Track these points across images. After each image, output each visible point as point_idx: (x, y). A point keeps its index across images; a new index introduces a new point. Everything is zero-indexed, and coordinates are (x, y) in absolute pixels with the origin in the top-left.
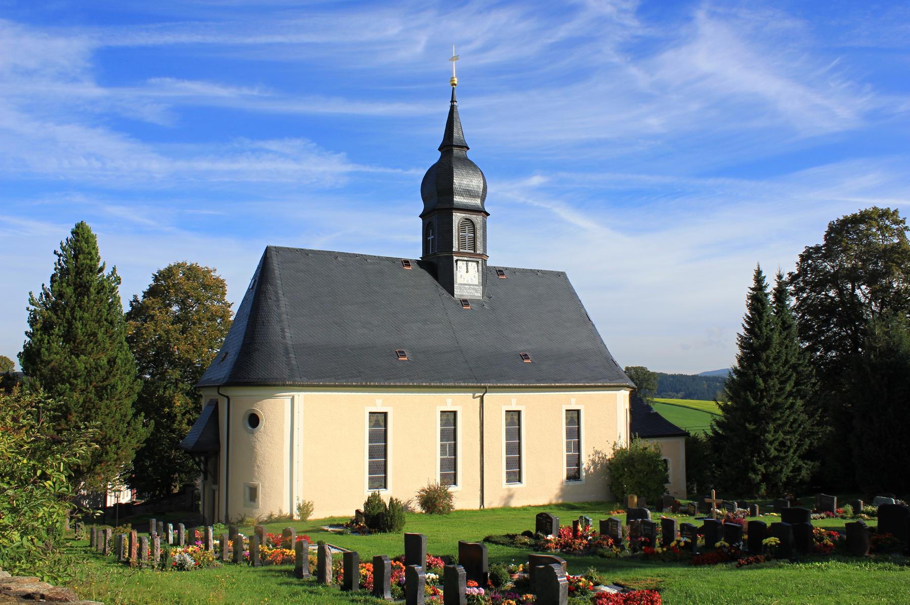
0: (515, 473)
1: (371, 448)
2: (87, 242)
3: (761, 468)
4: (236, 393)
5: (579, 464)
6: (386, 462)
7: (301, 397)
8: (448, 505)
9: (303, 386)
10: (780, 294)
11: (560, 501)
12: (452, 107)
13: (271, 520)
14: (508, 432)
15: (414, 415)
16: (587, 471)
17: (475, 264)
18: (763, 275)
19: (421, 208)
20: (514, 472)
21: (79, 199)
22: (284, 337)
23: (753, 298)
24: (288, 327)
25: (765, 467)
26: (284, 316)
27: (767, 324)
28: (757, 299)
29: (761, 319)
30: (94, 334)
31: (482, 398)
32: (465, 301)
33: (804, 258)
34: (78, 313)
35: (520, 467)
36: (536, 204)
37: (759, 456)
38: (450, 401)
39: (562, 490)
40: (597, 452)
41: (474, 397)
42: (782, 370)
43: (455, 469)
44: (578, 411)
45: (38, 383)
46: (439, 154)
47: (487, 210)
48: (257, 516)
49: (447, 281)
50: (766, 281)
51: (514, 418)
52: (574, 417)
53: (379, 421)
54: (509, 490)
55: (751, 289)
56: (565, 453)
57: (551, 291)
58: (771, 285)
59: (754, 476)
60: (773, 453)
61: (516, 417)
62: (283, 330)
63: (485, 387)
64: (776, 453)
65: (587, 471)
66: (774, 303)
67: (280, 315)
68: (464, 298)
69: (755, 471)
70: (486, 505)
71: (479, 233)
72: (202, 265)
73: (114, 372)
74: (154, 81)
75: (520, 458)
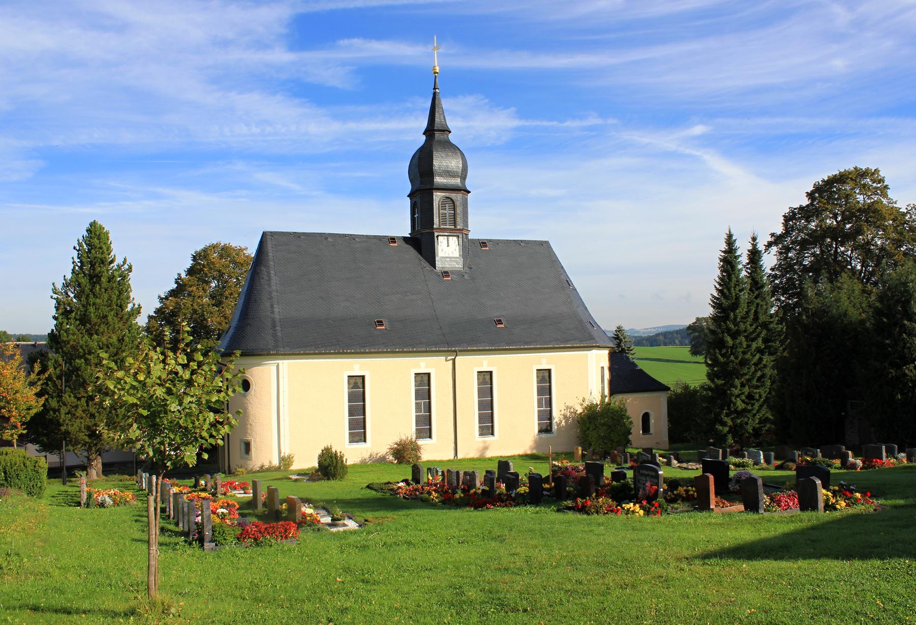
0: (487, 425)
1: (350, 407)
2: (99, 239)
5: (550, 418)
6: (364, 419)
7: (286, 364)
9: (285, 355)
10: (755, 255)
11: (534, 452)
12: (435, 94)
13: (262, 470)
15: (390, 378)
16: (558, 425)
17: (455, 238)
18: (734, 238)
19: (408, 188)
21: (240, 166)
22: (273, 312)
23: (725, 261)
24: (280, 303)
25: (732, 419)
26: (274, 293)
27: (736, 285)
28: (729, 261)
29: (731, 281)
30: (105, 317)
31: (454, 360)
32: (445, 272)
33: (787, 219)
34: (92, 300)
35: (492, 422)
36: (688, 151)
37: (729, 409)
38: (423, 364)
39: (536, 442)
40: (567, 407)
41: (446, 360)
42: (750, 329)
43: (430, 424)
44: (549, 371)
45: (60, 359)
46: (424, 138)
47: (469, 189)
48: (251, 467)
49: (429, 254)
50: (737, 244)
51: (486, 379)
52: (545, 377)
53: (357, 385)
54: (484, 442)
56: (536, 409)
57: (535, 260)
58: (743, 250)
59: (721, 428)
60: (740, 405)
61: (488, 377)
62: (272, 306)
63: (455, 351)
64: (744, 406)
65: (558, 425)
66: (748, 264)
67: (270, 293)
68: (446, 270)
69: (724, 424)
70: (460, 456)
71: (459, 210)
72: (234, 244)
73: (123, 348)
74: (345, 42)
75: (492, 413)
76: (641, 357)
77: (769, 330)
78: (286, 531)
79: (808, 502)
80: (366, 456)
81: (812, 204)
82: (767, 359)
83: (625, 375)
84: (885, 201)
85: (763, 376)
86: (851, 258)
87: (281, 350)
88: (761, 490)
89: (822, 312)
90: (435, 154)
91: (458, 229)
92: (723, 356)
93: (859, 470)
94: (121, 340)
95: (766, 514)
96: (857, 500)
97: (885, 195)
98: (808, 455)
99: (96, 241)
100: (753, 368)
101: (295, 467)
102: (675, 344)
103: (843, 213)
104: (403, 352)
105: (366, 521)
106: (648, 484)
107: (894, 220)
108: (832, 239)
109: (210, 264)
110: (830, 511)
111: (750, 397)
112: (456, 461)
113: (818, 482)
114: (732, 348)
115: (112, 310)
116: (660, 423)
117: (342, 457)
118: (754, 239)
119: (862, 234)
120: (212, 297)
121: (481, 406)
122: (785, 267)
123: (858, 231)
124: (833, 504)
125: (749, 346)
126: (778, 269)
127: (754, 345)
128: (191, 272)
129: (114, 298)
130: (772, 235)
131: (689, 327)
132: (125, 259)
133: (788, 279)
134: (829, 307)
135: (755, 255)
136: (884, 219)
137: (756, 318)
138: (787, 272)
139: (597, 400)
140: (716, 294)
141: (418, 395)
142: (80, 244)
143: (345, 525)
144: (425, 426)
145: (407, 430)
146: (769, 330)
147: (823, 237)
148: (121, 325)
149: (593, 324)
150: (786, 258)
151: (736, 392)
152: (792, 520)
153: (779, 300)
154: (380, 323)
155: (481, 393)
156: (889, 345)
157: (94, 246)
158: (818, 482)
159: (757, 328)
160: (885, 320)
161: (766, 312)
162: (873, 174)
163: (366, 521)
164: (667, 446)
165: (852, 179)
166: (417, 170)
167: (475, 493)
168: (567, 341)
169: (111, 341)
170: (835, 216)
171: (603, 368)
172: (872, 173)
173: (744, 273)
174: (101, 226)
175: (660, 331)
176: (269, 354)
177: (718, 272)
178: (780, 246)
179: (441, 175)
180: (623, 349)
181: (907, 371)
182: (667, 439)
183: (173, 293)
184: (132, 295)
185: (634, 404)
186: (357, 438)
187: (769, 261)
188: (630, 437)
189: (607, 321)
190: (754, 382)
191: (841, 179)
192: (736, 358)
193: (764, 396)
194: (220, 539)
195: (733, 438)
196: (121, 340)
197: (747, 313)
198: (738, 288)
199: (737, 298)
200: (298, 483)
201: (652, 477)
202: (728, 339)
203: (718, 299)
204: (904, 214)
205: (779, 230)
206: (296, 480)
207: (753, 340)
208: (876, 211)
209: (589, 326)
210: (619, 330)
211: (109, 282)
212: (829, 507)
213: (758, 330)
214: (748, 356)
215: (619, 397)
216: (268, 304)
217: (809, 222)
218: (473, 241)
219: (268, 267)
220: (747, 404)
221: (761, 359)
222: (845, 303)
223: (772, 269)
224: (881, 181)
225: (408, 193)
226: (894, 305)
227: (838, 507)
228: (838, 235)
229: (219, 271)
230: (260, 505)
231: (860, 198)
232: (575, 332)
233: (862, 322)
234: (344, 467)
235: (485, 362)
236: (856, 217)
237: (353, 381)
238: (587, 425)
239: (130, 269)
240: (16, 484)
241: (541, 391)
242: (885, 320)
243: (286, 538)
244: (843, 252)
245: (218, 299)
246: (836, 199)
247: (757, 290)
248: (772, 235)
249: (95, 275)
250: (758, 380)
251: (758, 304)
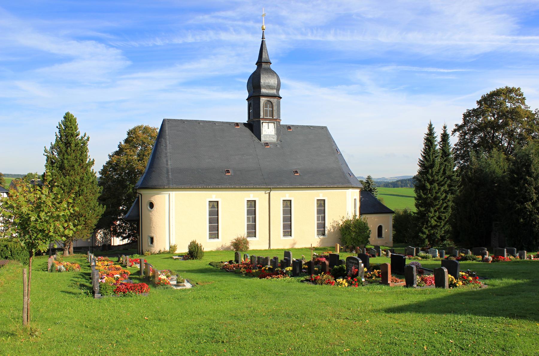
0: (288, 230)
3: (427, 231)
4: (143, 192)
8: (246, 247)
9: (173, 188)
10: (445, 137)
12: (262, 41)
14: (284, 211)
15: (232, 203)
17: (273, 124)
18: (433, 127)
19: (247, 96)
20: (288, 231)
22: (167, 165)
24: (171, 159)
25: (429, 230)
26: (168, 154)
27: (433, 154)
28: (429, 140)
29: (430, 151)
30: (73, 166)
31: (269, 193)
33: (465, 116)
34: (66, 156)
38: (252, 195)
41: (265, 193)
42: (441, 179)
46: (256, 66)
50: (435, 130)
51: (288, 204)
52: (321, 204)
53: (214, 207)
55: (427, 134)
56: (316, 222)
59: (422, 235)
60: (433, 223)
61: (289, 203)
62: (167, 161)
63: (270, 188)
66: (441, 142)
67: (166, 154)
69: (424, 233)
70: (271, 248)
71: (275, 108)
72: (151, 126)
76: (380, 194)
77: (452, 180)
78: (141, 289)
79: (440, 282)
80: (220, 246)
81: (480, 108)
82: (450, 196)
83: (370, 203)
84: (523, 107)
85: (447, 206)
86: (501, 139)
87: (171, 186)
88: (415, 273)
89: (480, 171)
90: (262, 76)
91: (274, 119)
92: (424, 194)
93: (490, 262)
94: (82, 179)
95: (419, 289)
96: (470, 281)
97: (523, 103)
98: (463, 253)
99: (69, 123)
100: (441, 202)
101: (178, 251)
102: (407, 186)
103: (498, 113)
104: (240, 188)
105: (197, 284)
106: (353, 268)
107: (527, 117)
108: (491, 129)
109: (137, 137)
110: (453, 287)
111: (439, 218)
112: (270, 250)
113: (446, 270)
114: (430, 190)
115: (77, 162)
116: (388, 232)
117: (201, 247)
118: (445, 127)
119: (508, 126)
120: (139, 155)
121: (285, 219)
122: (463, 144)
123: (506, 124)
124: (455, 283)
125: (439, 189)
126: (459, 145)
127: (442, 189)
128: (127, 141)
129: (78, 155)
130: (456, 125)
131: (414, 177)
132: (85, 134)
133: (465, 151)
134: (484, 168)
135: (445, 137)
136: (522, 117)
137: (444, 173)
138: (464, 147)
139: (351, 218)
140: (422, 159)
141: (249, 212)
142: (60, 125)
143: (184, 286)
144: (252, 230)
145: (242, 232)
146: (452, 180)
147: (486, 127)
148: (82, 170)
149: (351, 174)
150: (465, 138)
151: (431, 215)
152: (424, 293)
153: (459, 163)
154: (228, 171)
155: (285, 212)
156: (517, 190)
157: (68, 126)
158: (446, 270)
159: (444, 178)
160: (515, 176)
161: (450, 170)
162: (516, 91)
163: (197, 284)
164: (391, 244)
165: (504, 93)
166: (251, 85)
167: (265, 269)
168: (313, 184)
169: (76, 179)
170: (494, 116)
171: (355, 199)
172: (516, 91)
173: (438, 147)
174: (72, 115)
175: (399, 179)
176: (164, 188)
177: (423, 146)
178: (461, 132)
179: (265, 88)
180: (371, 189)
181: (527, 206)
182: (392, 241)
183: (117, 153)
184: (88, 154)
185: (373, 221)
186: (213, 236)
187: (454, 140)
188: (369, 239)
189: (360, 172)
190: (442, 210)
191: (497, 93)
192: (432, 196)
193: (447, 217)
194: (104, 292)
195: (429, 241)
196: (82, 179)
197: (439, 170)
198: (434, 156)
199: (434, 161)
200: (176, 261)
201: (355, 264)
202: (428, 185)
203: (423, 161)
204: (534, 115)
205: (461, 122)
206: (176, 259)
207: (442, 185)
208: (517, 112)
209: (348, 175)
210: (369, 178)
211: (75, 146)
212: (452, 285)
213: (445, 180)
214: (439, 195)
215: (364, 216)
216: (165, 160)
217: (478, 118)
218: (283, 126)
219: (165, 139)
220: (438, 222)
221: (446, 197)
222: (494, 166)
223: (456, 145)
224: (521, 95)
225: (247, 97)
226: (521, 168)
227: (457, 285)
228: (495, 126)
229: (142, 141)
230: (142, 273)
231: (508, 105)
232: (340, 178)
233: (503, 177)
234: (202, 253)
235: (287, 195)
236: (505, 116)
237: (212, 204)
238: (345, 232)
239: (88, 139)
240: (17, 258)
241: (319, 212)
242: (515, 176)
243: (142, 292)
244: (497, 136)
245: (141, 157)
246: (494, 105)
247: (445, 157)
248: (456, 125)
249: (69, 144)
250: (444, 209)
251: (446, 165)
